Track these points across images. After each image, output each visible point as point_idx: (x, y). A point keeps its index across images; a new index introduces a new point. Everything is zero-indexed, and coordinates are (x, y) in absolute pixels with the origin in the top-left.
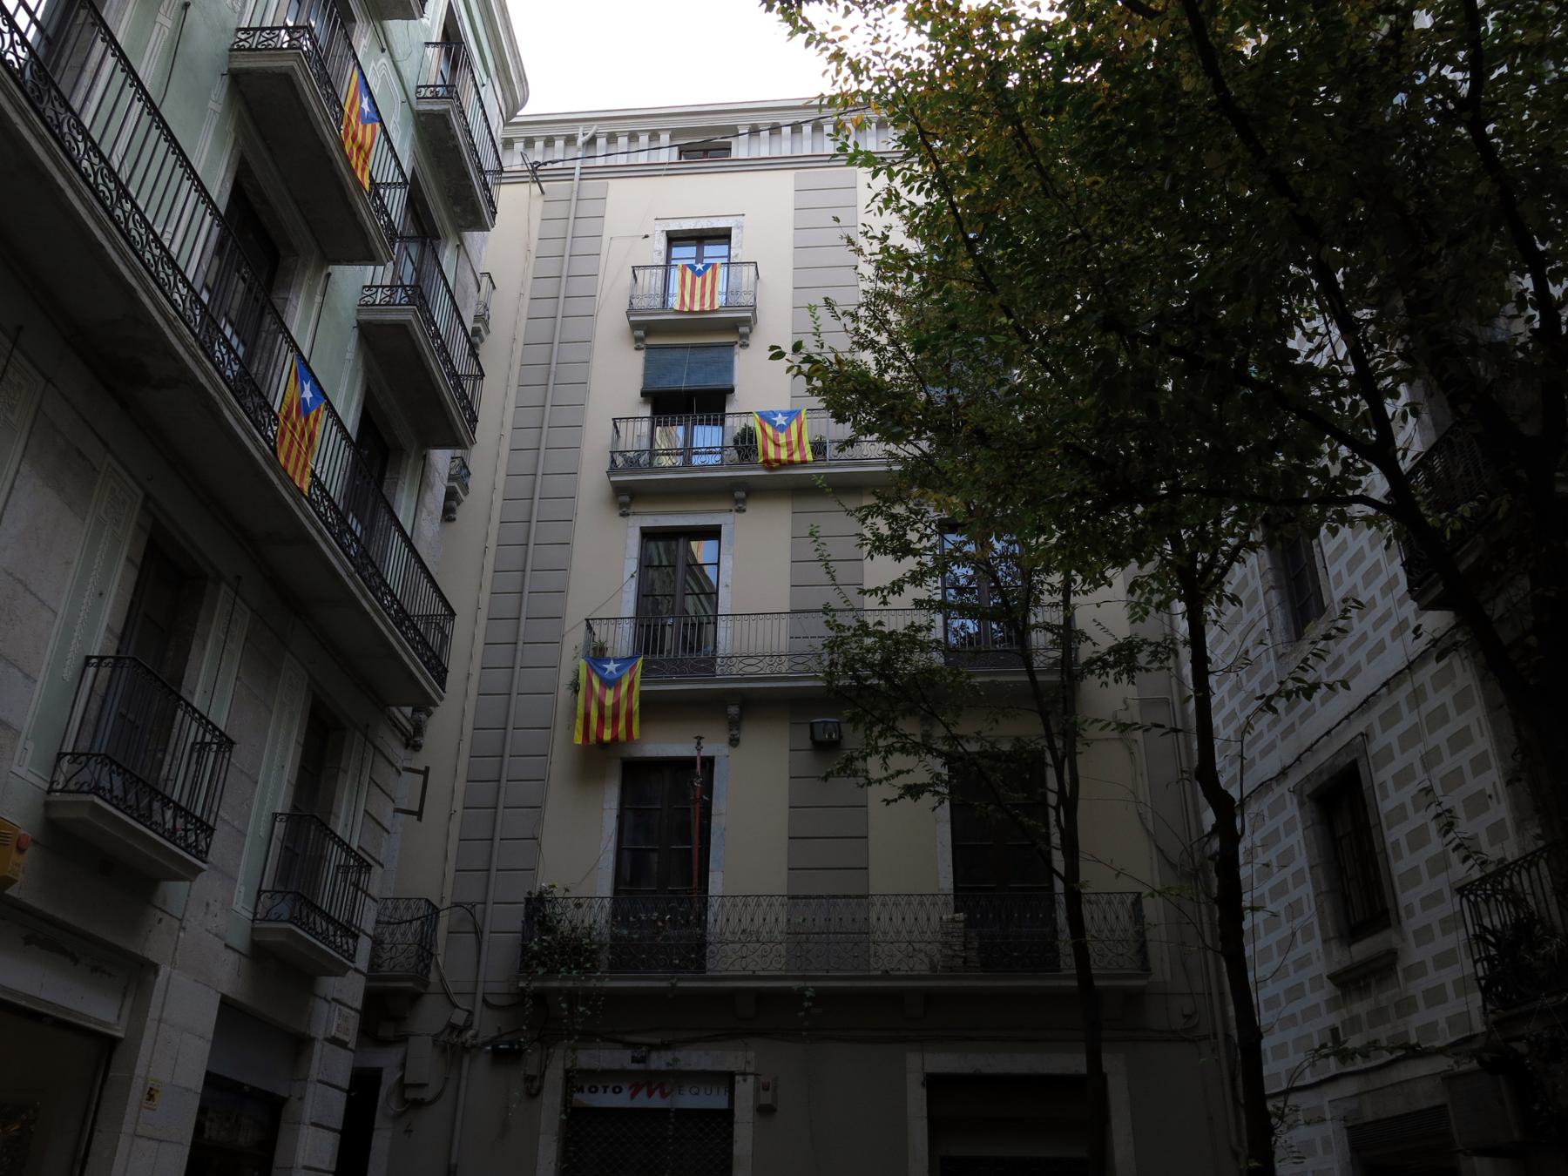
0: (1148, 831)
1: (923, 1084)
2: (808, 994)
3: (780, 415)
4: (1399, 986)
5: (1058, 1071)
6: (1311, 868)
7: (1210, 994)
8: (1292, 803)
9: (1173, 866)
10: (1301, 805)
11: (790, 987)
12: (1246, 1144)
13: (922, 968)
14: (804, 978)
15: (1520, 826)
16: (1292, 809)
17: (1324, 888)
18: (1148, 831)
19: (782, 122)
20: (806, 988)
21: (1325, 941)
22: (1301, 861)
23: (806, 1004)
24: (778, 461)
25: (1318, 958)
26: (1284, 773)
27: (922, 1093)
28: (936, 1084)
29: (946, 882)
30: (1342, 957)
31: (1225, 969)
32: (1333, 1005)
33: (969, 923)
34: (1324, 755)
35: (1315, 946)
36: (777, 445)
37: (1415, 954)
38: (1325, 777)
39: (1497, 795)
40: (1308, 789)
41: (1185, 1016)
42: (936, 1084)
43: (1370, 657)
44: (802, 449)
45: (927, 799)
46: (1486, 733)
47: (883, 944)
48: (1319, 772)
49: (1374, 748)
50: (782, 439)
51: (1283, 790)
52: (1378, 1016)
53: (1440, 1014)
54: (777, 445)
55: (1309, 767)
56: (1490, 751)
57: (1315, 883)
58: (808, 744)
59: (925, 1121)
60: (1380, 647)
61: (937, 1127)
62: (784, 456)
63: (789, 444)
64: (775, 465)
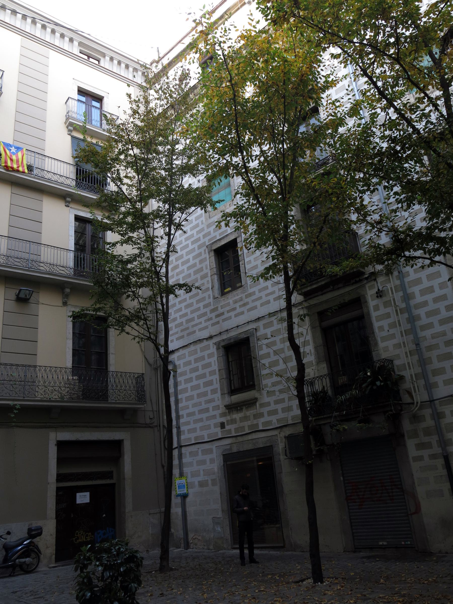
0: (142, 350)
1: (56, 445)
2: (17, 407)
3: (13, 147)
4: (256, 409)
5: (107, 439)
6: (219, 370)
7: (159, 411)
8: (213, 348)
9: (150, 365)
10: (218, 349)
11: (8, 404)
12: (166, 463)
13: (55, 396)
14: (13, 400)
15: (318, 363)
16: (213, 349)
17: (224, 377)
18: (142, 350)
19: (18, 11)
20: (16, 405)
21: (222, 394)
22: (215, 367)
23: (15, 411)
24: (12, 168)
25: (218, 400)
26: (211, 337)
27: (55, 448)
28: (60, 444)
29: (69, 364)
30: (228, 400)
31: (164, 402)
32: (223, 415)
33: (80, 379)
34: (233, 334)
35: (219, 394)
36: (11, 160)
37: (265, 399)
38: (232, 341)
39: (311, 353)
40: (223, 344)
41: (150, 419)
42: (60, 444)
43: (262, 305)
44: (23, 167)
45: (126, 331)
46: (309, 334)
47: (48, 387)
48: (230, 339)
49: (259, 334)
50: (14, 157)
51: (211, 342)
52: (246, 418)
53: (274, 418)
54: (11, 160)
55: (224, 337)
56: (310, 340)
57: (220, 375)
58: (14, 297)
59: (56, 460)
60: (268, 302)
61: (60, 461)
62: (15, 166)
63: (17, 161)
64: (10, 169)
